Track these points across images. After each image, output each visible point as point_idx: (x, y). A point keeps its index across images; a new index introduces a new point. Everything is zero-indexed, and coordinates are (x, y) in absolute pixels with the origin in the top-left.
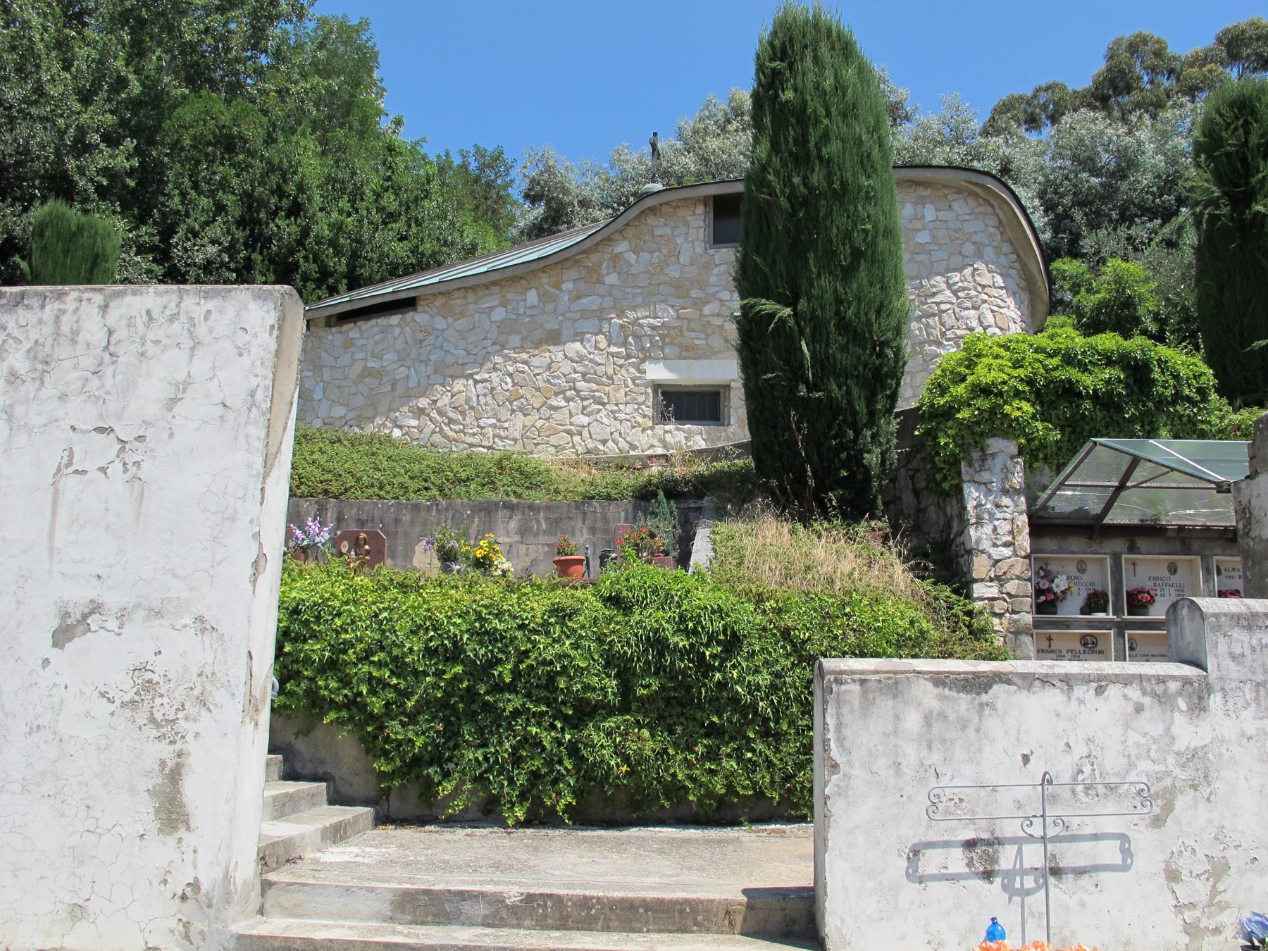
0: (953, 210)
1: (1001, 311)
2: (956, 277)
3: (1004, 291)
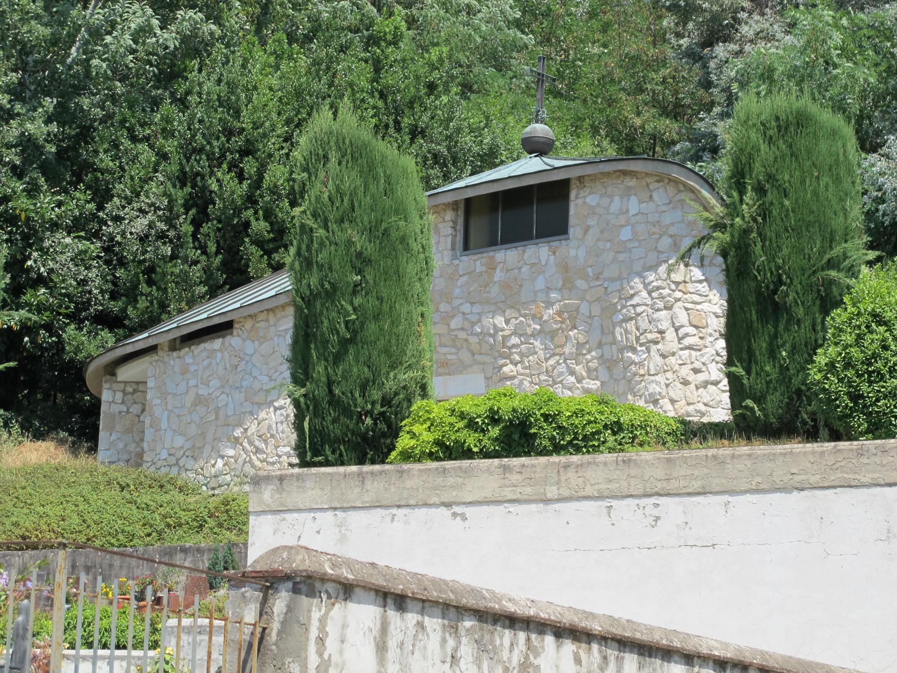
0: (654, 201)
1: (699, 307)
2: (651, 277)
3: (705, 284)
